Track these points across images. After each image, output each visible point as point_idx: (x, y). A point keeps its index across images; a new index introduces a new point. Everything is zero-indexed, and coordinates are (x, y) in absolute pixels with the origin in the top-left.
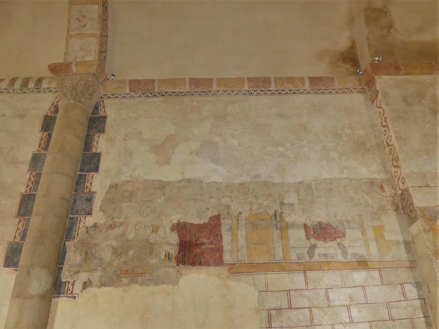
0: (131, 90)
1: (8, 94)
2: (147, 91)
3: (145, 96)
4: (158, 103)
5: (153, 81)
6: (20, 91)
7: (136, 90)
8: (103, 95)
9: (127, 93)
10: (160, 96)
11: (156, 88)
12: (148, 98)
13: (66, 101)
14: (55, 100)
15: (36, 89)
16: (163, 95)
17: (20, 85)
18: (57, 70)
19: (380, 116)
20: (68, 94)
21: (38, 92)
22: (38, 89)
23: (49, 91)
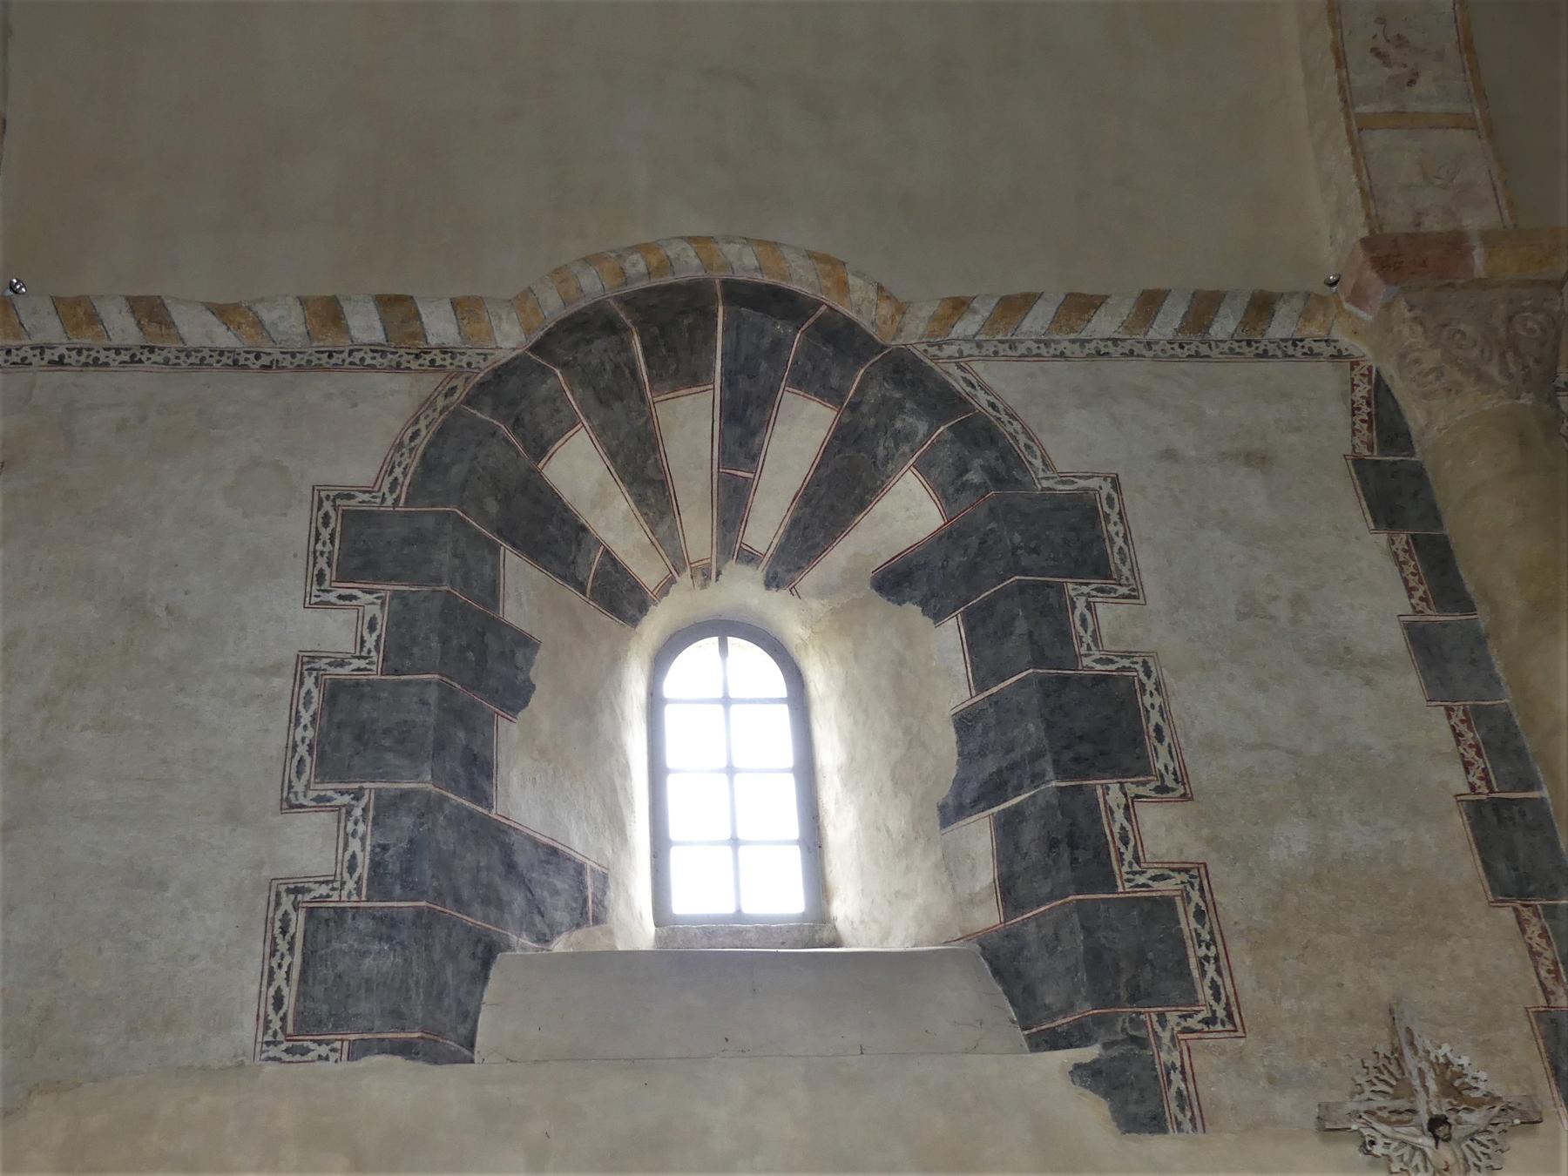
17: (1177, 324)
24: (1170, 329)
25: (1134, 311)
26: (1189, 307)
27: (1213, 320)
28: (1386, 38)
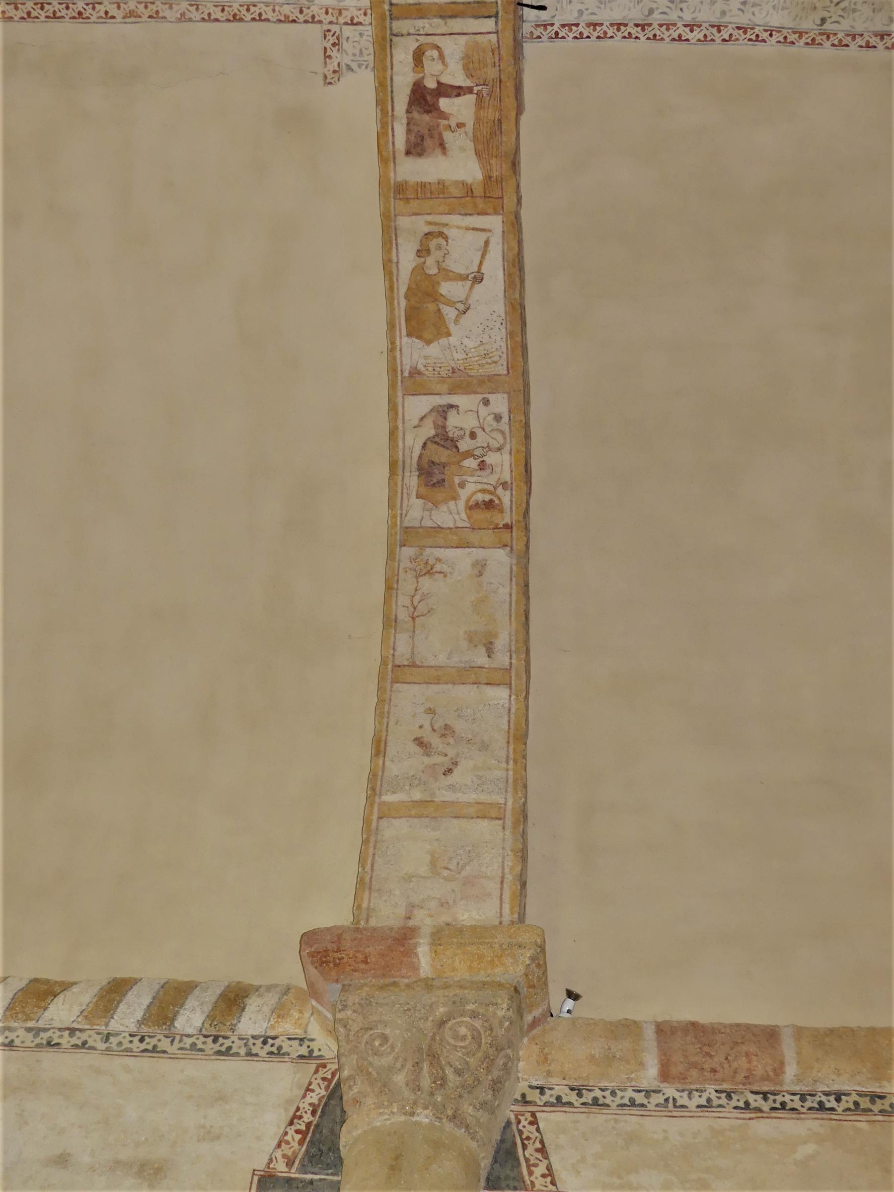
0: (665, 1075)
1: (81, 1055)
2: (744, 1084)
3: (735, 1108)
4: (810, 1149)
5: (771, 1035)
6: (136, 1045)
7: (694, 1073)
8: (531, 1087)
9: (645, 1085)
10: (810, 1109)
11: (791, 1071)
12: (750, 1119)
13: (393, 1113)
14: (304, 1096)
15: (212, 1038)
16: (821, 1107)
17: (139, 1015)
18: (345, 960)
19: (369, 1047)
20: (400, 1079)
21: (219, 1053)
22: (221, 1039)
23: (272, 1053)
24: (132, 1020)
25: (95, 1000)
26: (154, 998)
27: (178, 1012)
28: (432, 727)
